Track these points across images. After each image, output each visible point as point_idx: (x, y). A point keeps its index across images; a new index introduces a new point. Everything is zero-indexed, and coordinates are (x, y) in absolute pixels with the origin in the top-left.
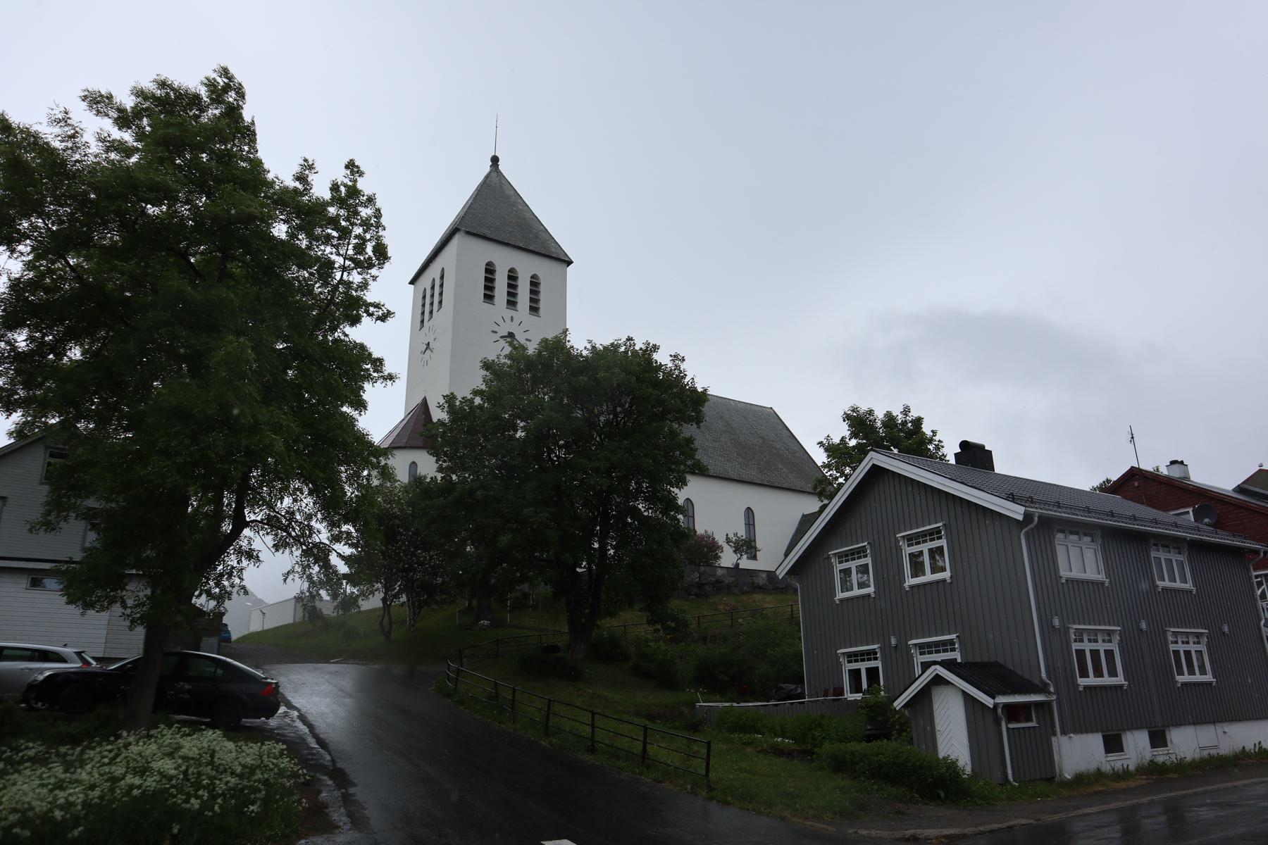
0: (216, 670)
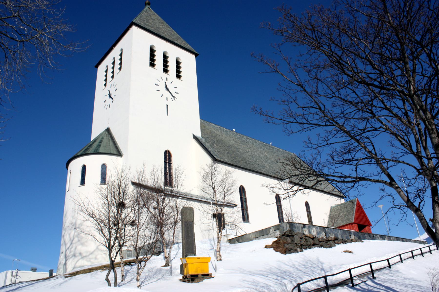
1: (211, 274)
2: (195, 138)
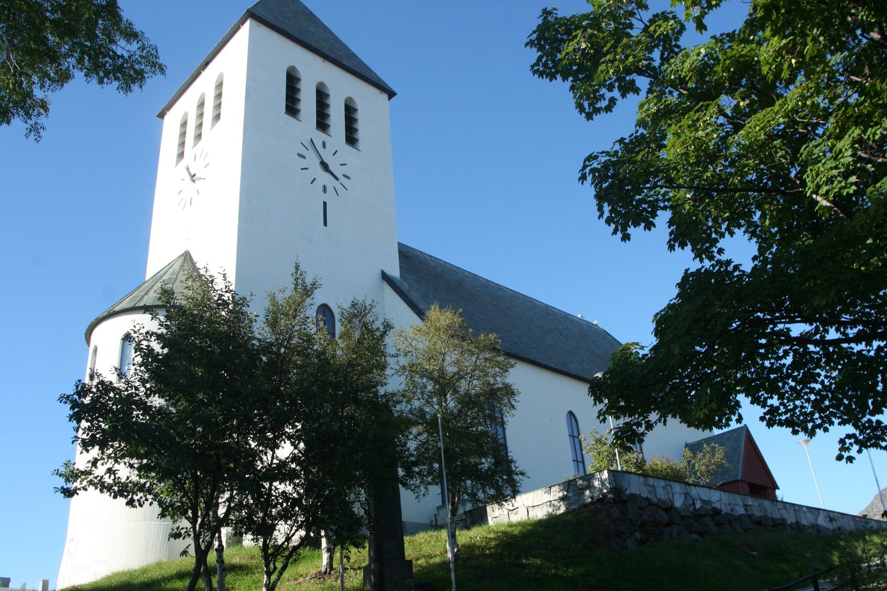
2: (385, 277)
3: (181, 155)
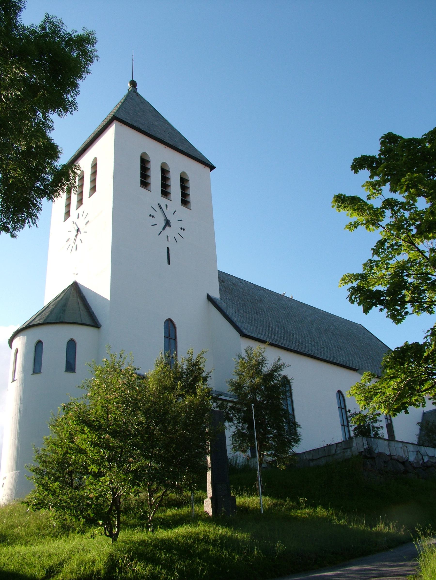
0: (408, 302)
1: (397, 324)
2: (210, 298)
3: (68, 214)
